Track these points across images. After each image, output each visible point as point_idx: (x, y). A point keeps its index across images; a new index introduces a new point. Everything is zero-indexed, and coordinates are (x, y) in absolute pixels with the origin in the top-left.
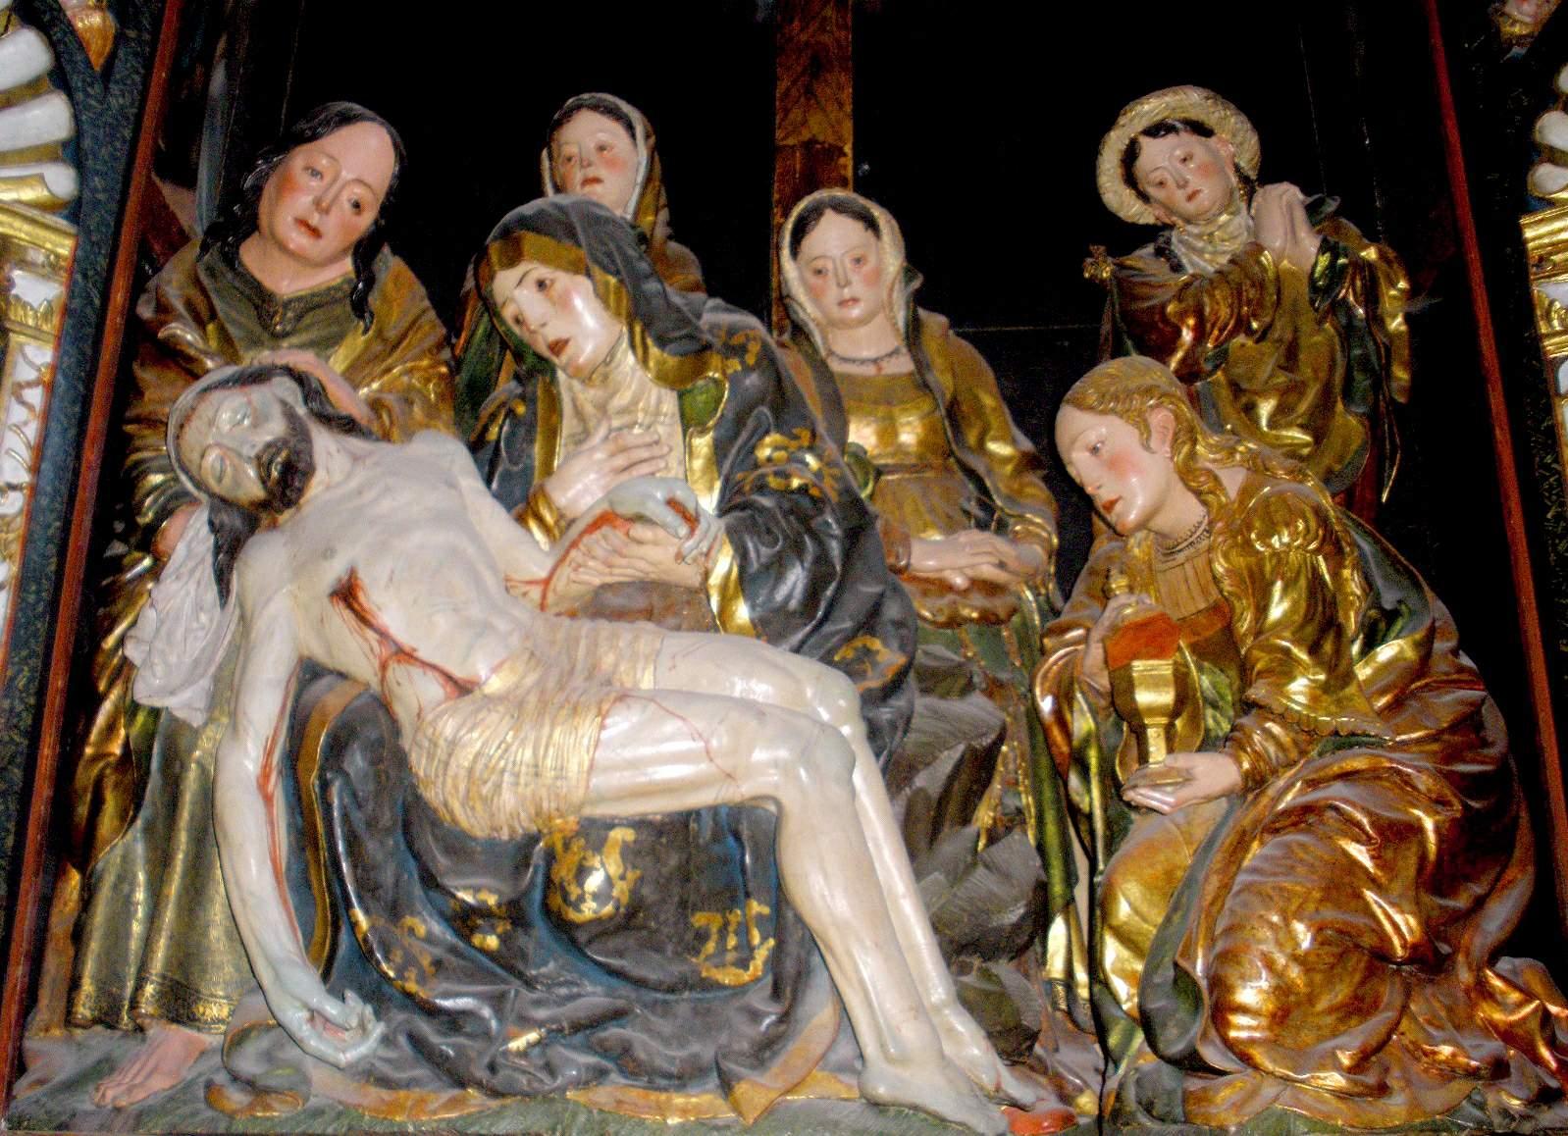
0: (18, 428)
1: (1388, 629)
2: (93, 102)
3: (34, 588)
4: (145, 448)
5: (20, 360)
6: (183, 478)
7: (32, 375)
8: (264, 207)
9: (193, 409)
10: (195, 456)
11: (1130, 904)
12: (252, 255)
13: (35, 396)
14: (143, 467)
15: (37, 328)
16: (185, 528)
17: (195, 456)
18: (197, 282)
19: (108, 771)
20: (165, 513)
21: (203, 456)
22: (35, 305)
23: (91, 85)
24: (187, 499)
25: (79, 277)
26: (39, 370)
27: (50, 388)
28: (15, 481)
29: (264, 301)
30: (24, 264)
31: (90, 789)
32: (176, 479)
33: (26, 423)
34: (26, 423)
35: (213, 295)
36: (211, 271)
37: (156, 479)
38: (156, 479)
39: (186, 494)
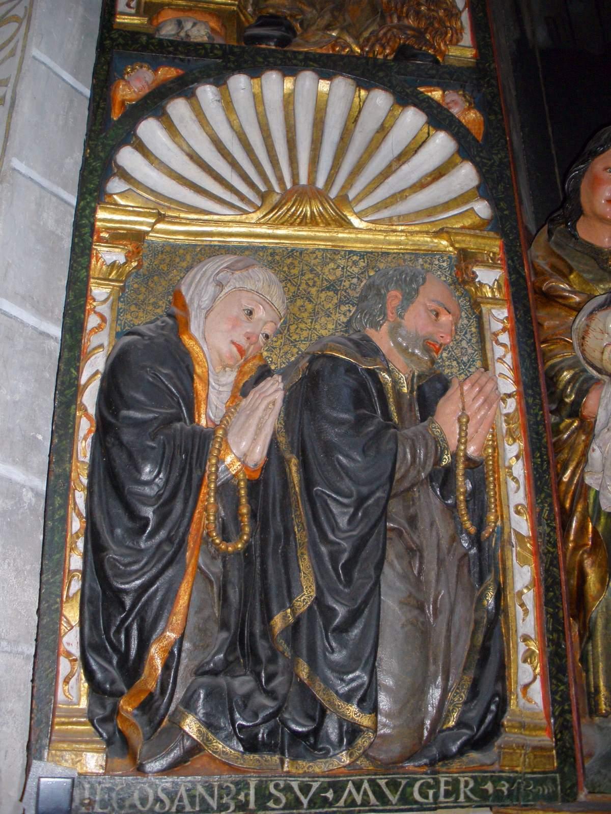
0: (501, 359)
1: (84, 315)
2: (485, 161)
3: (538, 455)
4: (555, 356)
5: (492, 320)
6: (590, 369)
7: (501, 326)
8: (584, 199)
9: (588, 326)
10: (597, 354)
11: (413, 571)
12: (585, 230)
13: (505, 338)
14: (557, 369)
15: (494, 298)
16: (599, 399)
17: (597, 354)
18: (553, 253)
19: (585, 556)
20: (582, 393)
21: (602, 353)
22: (491, 284)
23: (481, 151)
24: (592, 382)
25: (510, 262)
26: (503, 322)
27: (511, 332)
28: (509, 392)
29: (598, 255)
30: (477, 262)
31: (576, 568)
32: (585, 371)
33: (504, 356)
34: (504, 356)
35: (565, 258)
36: (557, 244)
37: (567, 375)
38: (567, 375)
39: (592, 378)
